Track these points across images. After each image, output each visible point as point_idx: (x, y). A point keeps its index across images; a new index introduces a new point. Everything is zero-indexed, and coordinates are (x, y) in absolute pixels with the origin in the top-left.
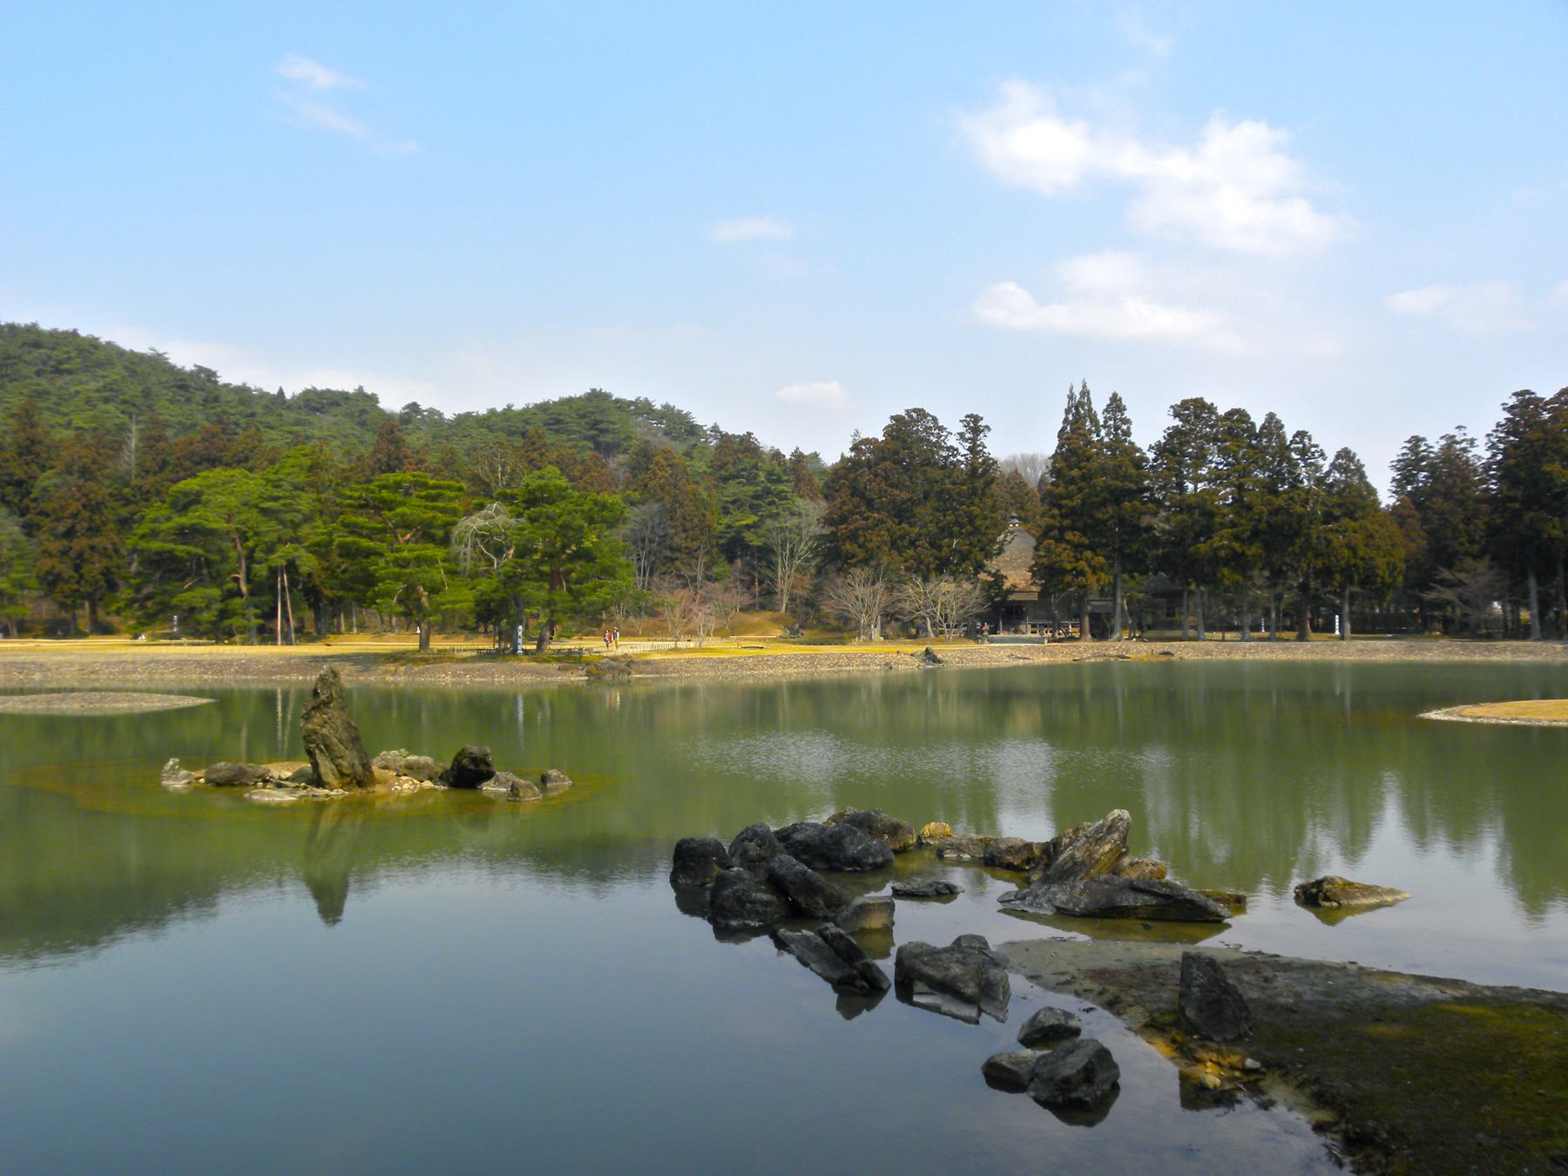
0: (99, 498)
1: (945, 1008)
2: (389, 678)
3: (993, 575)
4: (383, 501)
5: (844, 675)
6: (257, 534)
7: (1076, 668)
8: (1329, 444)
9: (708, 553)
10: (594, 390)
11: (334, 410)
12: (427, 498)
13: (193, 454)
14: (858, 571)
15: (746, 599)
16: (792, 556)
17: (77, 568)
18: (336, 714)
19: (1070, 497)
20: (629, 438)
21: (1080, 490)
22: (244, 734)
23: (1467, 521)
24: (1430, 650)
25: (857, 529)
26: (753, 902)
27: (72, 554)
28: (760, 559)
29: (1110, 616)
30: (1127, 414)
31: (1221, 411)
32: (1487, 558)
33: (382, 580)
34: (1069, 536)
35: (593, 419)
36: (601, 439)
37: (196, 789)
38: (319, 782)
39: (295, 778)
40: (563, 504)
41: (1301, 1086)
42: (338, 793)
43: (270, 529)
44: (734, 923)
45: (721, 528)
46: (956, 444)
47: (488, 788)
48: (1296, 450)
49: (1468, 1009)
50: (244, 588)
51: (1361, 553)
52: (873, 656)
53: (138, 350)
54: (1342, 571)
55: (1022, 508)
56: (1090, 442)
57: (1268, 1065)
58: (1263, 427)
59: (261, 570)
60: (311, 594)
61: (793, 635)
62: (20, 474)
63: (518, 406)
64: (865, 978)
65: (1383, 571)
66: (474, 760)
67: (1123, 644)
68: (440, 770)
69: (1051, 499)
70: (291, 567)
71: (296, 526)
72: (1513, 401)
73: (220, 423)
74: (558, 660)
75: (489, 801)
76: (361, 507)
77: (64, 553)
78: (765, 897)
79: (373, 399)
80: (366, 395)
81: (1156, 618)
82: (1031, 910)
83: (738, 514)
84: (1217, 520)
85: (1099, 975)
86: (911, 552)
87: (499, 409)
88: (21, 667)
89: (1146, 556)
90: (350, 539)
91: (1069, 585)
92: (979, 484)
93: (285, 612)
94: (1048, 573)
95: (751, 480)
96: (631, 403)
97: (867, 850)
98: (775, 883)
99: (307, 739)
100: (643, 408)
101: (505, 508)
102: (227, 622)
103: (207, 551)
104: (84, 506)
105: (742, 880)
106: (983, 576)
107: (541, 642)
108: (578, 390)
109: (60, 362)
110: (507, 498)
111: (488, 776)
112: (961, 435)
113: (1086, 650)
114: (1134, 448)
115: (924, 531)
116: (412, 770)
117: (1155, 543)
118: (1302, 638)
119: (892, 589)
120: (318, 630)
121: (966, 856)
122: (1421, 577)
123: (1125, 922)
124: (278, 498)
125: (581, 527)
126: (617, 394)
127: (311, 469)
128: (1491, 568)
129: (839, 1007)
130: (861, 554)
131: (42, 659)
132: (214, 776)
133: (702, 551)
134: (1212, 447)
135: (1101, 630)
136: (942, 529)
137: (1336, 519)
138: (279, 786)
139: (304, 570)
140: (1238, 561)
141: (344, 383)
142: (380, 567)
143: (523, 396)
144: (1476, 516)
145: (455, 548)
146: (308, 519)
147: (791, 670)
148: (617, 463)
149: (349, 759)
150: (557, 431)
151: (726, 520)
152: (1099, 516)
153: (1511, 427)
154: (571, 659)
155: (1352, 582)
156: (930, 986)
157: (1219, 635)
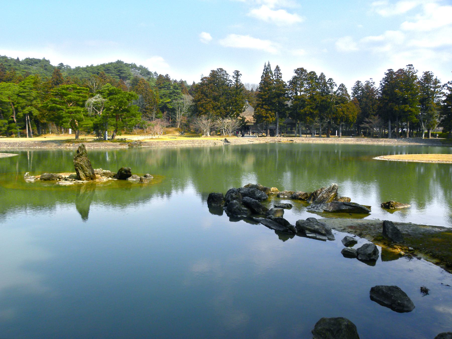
1: (318, 237)
2: (68, 147)
4: (63, 93)
5: (202, 146)
6: (18, 103)
7: (265, 145)
8: (338, 82)
9: (156, 110)
10: (118, 60)
11: (36, 65)
14: (203, 116)
15: (168, 124)
16: (181, 111)
18: (84, 158)
19: (265, 95)
20: (130, 75)
21: (268, 93)
22: (17, 165)
23: (373, 105)
24: (363, 141)
25: (203, 104)
26: (243, 210)
28: (171, 112)
29: (275, 129)
30: (281, 72)
31: (308, 72)
32: (378, 116)
33: (65, 118)
34: (264, 107)
35: (118, 70)
36: (121, 75)
39: (71, 177)
42: (85, 182)
43: (23, 102)
44: (239, 216)
45: (160, 103)
46: (232, 79)
47: (130, 179)
48: (329, 83)
50: (15, 120)
51: (345, 113)
52: (207, 141)
55: (248, 98)
57: (415, 249)
58: (320, 77)
59: (21, 114)
61: (182, 134)
63: (95, 65)
64: (290, 230)
65: (351, 119)
66: (126, 171)
67: (279, 138)
68: (113, 174)
69: (259, 96)
70: (30, 114)
72: (388, 72)
74: (119, 142)
75: (130, 184)
76: (56, 95)
78: (246, 209)
80: (46, 60)
81: (288, 130)
82: (317, 211)
83: (165, 99)
84: (306, 103)
86: (218, 110)
87: (89, 66)
89: (285, 113)
90: (54, 105)
91: (264, 120)
92: (238, 91)
93: (29, 127)
94: (258, 117)
95: (169, 88)
96: (130, 65)
97: (262, 195)
98: (246, 204)
99: (76, 166)
100: (134, 66)
102: (10, 131)
103: (3, 108)
106: (239, 118)
108: (114, 60)
110: (101, 93)
111: (130, 176)
112: (233, 76)
114: (283, 82)
116: (105, 174)
118: (328, 137)
120: (39, 133)
122: (360, 121)
123: (344, 214)
125: (126, 102)
127: (34, 83)
128: (379, 118)
129: (280, 238)
132: (44, 177)
133: (154, 109)
134: (305, 82)
135: (273, 134)
136: (228, 104)
137: (339, 103)
138: (66, 179)
139: (34, 114)
140: (312, 115)
142: (64, 114)
146: (35, 99)
149: (88, 172)
150: (108, 73)
151: (161, 100)
153: (386, 80)
154: (123, 141)
157: (305, 136)
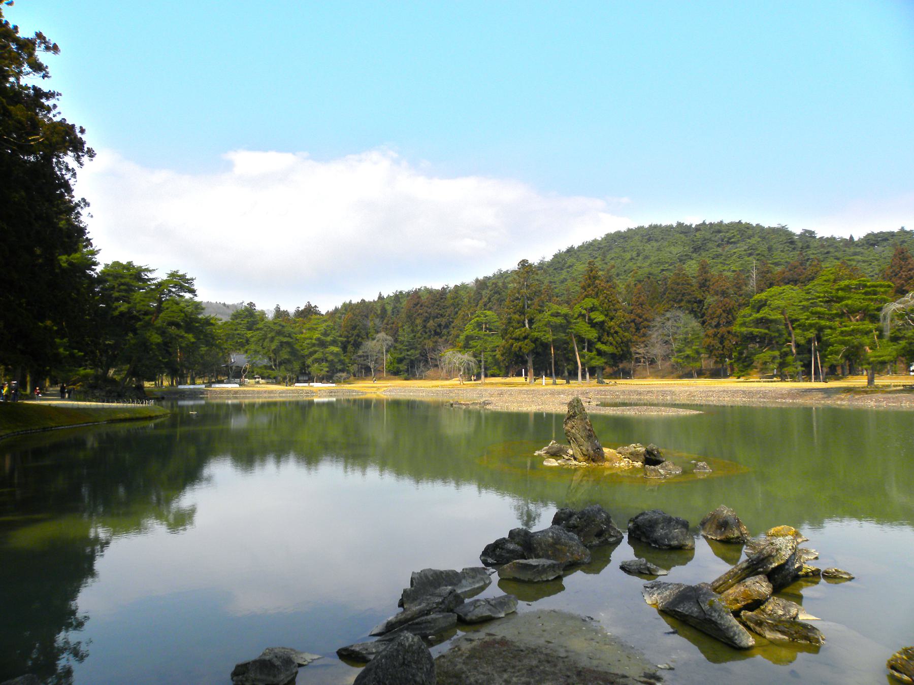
0: (731, 306)
12: (866, 293)
13: (784, 278)
17: (721, 343)
27: (719, 336)
50: (794, 351)
53: (772, 226)
62: (700, 297)
73: (797, 257)
77: (715, 335)
79: (811, 233)
88: (664, 393)
104: (724, 311)
109: (730, 239)
131: (673, 389)
143: (693, 219)
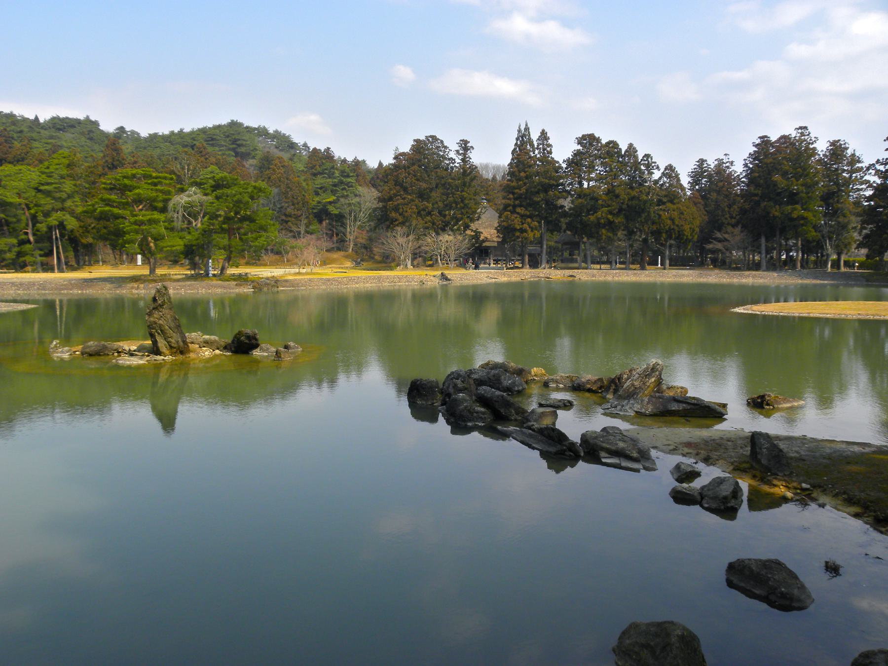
2: (135, 291)
3: (475, 231)
4: (126, 186)
5: (397, 287)
6: (36, 205)
7: (520, 284)
10: (232, 121)
11: (72, 130)
14: (399, 229)
15: (330, 245)
18: (167, 311)
21: (525, 184)
22: (36, 326)
23: (730, 206)
24: (710, 276)
25: (398, 205)
30: (550, 142)
31: (604, 142)
33: (129, 233)
34: (518, 210)
37: (74, 358)
38: (157, 352)
40: (236, 188)
41: (836, 496)
42: (169, 358)
43: (47, 202)
44: (470, 424)
45: (314, 203)
47: (256, 353)
49: (878, 456)
51: (677, 223)
52: (407, 277)
54: (667, 232)
55: (487, 194)
56: (530, 157)
58: (626, 151)
59: (43, 227)
60: (73, 242)
61: (358, 264)
63: (187, 129)
64: (570, 450)
65: (687, 233)
66: (248, 337)
67: (547, 271)
68: (223, 344)
69: (508, 189)
70: (61, 226)
71: (63, 201)
74: (234, 280)
75: (257, 362)
76: (111, 189)
78: (482, 409)
79: (96, 124)
80: (91, 121)
81: (565, 255)
82: (621, 413)
83: (324, 195)
84: (600, 202)
85: (689, 445)
86: (429, 218)
91: (518, 237)
92: (468, 179)
93: (58, 253)
94: (506, 231)
96: (255, 129)
97: (514, 383)
98: (483, 401)
100: (262, 132)
101: (198, 191)
102: (22, 259)
105: (466, 401)
106: (468, 232)
107: (223, 269)
108: (224, 120)
110: (199, 185)
111: (256, 346)
112: (457, 151)
113: (526, 274)
114: (554, 162)
115: (436, 206)
116: (207, 343)
117: (565, 214)
118: (643, 268)
119: (418, 239)
120: (78, 263)
121: (561, 386)
122: (706, 237)
124: (52, 183)
126: (246, 124)
128: (742, 232)
130: (401, 219)
132: (88, 350)
133: (304, 216)
135: (534, 263)
136: (446, 205)
137: (664, 203)
138: (131, 354)
139: (69, 227)
140: (610, 225)
141: (78, 114)
142: (126, 225)
143: (190, 124)
144: (734, 203)
145: (170, 214)
146: (70, 196)
147: (368, 285)
148: (251, 164)
150: (212, 145)
151: (317, 199)
152: (536, 199)
154: (241, 279)
155: (671, 238)
156: (609, 454)
157: (598, 266)
